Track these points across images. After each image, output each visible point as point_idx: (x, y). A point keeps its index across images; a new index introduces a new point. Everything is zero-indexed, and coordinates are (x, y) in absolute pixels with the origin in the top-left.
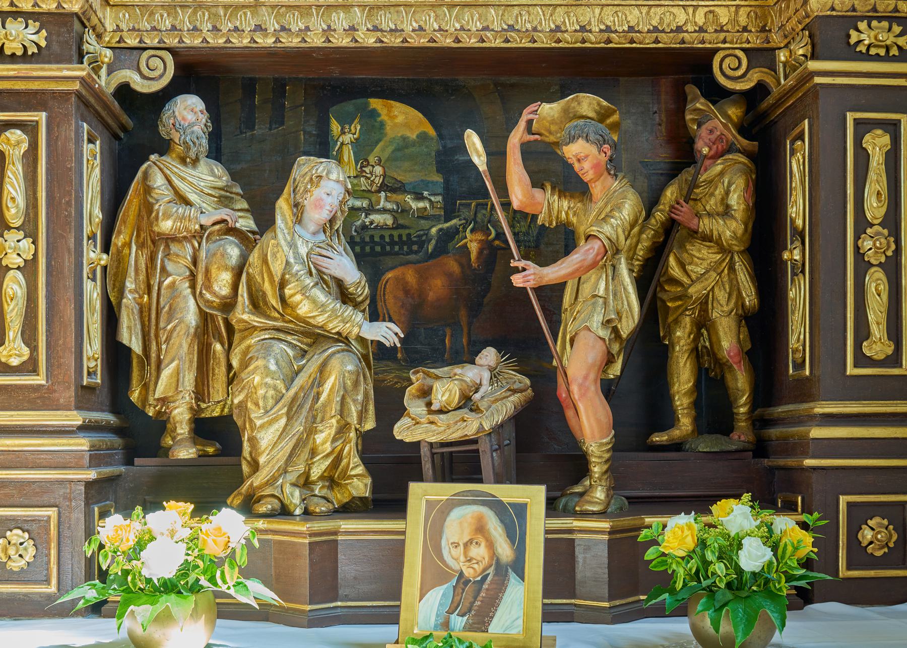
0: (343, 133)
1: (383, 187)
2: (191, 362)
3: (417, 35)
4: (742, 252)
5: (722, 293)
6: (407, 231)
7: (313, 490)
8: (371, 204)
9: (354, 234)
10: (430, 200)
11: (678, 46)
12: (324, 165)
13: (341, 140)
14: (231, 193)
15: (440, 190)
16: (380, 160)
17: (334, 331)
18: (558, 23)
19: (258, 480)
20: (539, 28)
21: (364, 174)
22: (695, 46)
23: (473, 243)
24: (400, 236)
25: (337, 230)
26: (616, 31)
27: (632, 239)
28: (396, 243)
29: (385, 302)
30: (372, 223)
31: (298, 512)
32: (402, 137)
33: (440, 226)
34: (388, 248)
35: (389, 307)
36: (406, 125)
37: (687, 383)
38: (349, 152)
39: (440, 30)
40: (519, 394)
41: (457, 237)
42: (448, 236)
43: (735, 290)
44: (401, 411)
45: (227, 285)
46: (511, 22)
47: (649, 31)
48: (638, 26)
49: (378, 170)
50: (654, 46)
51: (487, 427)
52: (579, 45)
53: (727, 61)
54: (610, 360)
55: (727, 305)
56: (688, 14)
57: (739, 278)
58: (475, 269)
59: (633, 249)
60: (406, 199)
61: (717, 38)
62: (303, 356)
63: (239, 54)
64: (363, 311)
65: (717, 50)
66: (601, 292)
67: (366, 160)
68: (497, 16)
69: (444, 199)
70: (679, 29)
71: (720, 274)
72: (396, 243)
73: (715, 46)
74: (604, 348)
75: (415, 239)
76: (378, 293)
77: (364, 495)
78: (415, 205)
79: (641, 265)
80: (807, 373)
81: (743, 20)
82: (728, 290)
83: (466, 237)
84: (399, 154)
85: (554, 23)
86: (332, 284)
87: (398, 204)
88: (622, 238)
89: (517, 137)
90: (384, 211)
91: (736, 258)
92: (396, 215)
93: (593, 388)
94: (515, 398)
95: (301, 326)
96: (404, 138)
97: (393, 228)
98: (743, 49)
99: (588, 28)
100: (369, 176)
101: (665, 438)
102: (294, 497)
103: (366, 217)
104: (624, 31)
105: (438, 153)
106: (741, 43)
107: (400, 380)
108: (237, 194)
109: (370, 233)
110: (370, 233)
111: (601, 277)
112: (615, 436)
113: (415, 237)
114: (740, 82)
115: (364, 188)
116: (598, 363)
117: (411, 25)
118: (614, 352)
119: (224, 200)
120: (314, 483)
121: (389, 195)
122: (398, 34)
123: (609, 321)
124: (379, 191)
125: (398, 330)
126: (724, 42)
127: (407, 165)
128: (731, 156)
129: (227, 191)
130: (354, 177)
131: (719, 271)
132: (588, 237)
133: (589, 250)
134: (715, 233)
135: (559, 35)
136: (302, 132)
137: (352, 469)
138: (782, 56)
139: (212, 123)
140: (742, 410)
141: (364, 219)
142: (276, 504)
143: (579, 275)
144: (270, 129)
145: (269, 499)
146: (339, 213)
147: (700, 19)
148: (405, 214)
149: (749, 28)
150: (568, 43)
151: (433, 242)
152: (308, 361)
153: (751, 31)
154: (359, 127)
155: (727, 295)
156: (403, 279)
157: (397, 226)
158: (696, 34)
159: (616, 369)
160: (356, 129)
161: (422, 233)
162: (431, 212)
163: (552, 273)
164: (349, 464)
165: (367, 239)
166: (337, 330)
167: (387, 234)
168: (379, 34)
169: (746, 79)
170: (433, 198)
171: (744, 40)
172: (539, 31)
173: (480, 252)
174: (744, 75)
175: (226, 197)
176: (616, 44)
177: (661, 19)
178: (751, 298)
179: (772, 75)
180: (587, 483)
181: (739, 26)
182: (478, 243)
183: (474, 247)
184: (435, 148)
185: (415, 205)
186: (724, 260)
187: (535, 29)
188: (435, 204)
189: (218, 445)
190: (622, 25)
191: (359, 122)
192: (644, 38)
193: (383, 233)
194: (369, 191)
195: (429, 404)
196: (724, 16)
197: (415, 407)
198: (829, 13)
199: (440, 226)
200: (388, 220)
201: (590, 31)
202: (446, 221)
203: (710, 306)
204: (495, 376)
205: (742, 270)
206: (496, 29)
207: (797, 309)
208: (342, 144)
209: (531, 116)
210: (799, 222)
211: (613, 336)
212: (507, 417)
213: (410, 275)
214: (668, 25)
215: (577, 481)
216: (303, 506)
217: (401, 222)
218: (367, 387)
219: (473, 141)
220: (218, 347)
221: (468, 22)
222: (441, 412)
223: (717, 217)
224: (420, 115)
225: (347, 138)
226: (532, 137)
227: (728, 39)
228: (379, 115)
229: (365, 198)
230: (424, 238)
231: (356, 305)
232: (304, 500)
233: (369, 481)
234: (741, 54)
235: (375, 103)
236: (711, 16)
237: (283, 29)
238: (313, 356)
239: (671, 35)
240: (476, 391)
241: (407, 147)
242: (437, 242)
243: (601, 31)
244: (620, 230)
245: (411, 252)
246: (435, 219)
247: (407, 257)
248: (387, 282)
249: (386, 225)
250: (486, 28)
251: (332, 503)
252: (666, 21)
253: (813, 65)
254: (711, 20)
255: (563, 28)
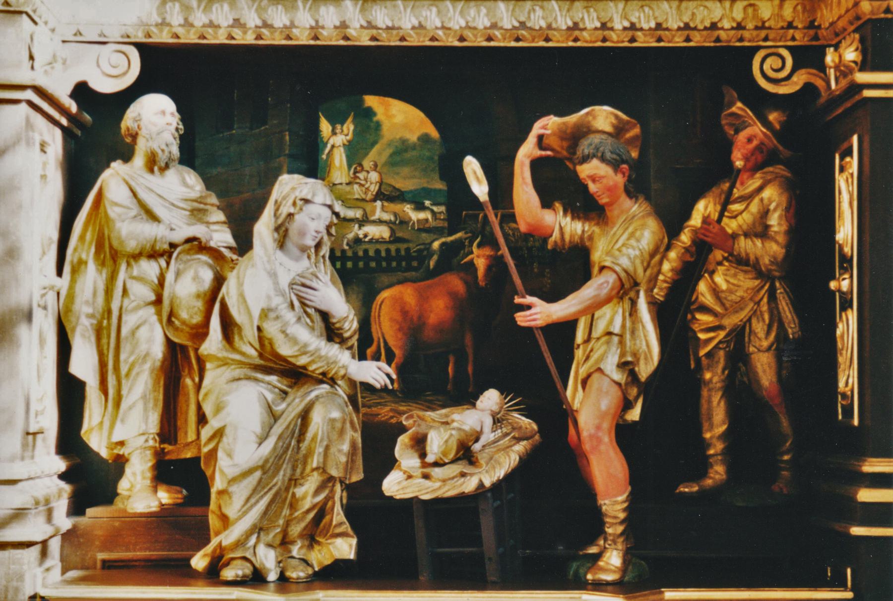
0: (334, 133)
1: (380, 196)
2: (156, 400)
3: (417, 34)
4: (780, 278)
5: (761, 324)
6: (405, 246)
7: (290, 551)
8: (365, 214)
9: (346, 247)
10: (432, 211)
11: (712, 44)
12: (309, 186)
13: (331, 142)
14: (206, 204)
15: (442, 200)
16: (376, 165)
17: (317, 372)
18: (577, 19)
19: (228, 538)
20: (554, 26)
21: (358, 181)
22: (732, 44)
23: (480, 259)
24: (398, 251)
25: (323, 257)
26: (641, 29)
27: (653, 268)
28: (393, 259)
29: (380, 325)
30: (366, 236)
31: (272, 577)
32: (401, 139)
33: (443, 240)
34: (384, 264)
35: (384, 331)
36: (405, 126)
37: (721, 425)
38: (341, 156)
39: (443, 28)
40: (524, 443)
41: (462, 252)
42: (451, 252)
43: (776, 317)
44: (390, 463)
45: (199, 314)
46: (522, 19)
47: (679, 29)
48: (667, 23)
49: (374, 176)
50: (685, 44)
51: (487, 483)
52: (599, 44)
53: (769, 61)
54: (627, 405)
55: (766, 338)
56: (725, 9)
57: (780, 307)
58: (483, 288)
59: (653, 281)
60: (405, 209)
61: (758, 36)
62: (284, 399)
63: (139, 560)
64: (350, 348)
65: (758, 48)
66: (616, 329)
67: (361, 165)
68: (507, 11)
69: (448, 210)
70: (714, 26)
71: (758, 303)
72: (393, 259)
73: (754, 44)
74: (620, 393)
75: (414, 254)
76: (372, 314)
77: (347, 557)
78: (415, 216)
79: (669, 288)
80: (856, 422)
81: (788, 12)
82: (767, 321)
83: (472, 253)
84: (398, 159)
85: (571, 19)
86: (317, 317)
87: (395, 215)
88: (640, 271)
89: (527, 151)
90: (380, 222)
91: (778, 284)
92: (394, 227)
93: (606, 439)
94: (521, 447)
95: (281, 365)
96: (404, 141)
97: (390, 242)
98: (788, 48)
99: (609, 25)
100: (363, 182)
101: (696, 489)
102: (267, 559)
103: (360, 228)
104: (650, 29)
105: (442, 158)
106: (786, 41)
107: (396, 415)
108: (212, 205)
109: (364, 247)
110: (364, 247)
111: (617, 312)
112: (631, 493)
113: (414, 252)
114: (782, 85)
115: (357, 196)
116: (612, 411)
117: (410, 21)
118: (631, 398)
119: (197, 213)
120: (293, 542)
121: (386, 204)
122: (395, 32)
123: (626, 364)
124: (374, 200)
125: (390, 370)
126: (766, 39)
127: (406, 170)
128: (771, 169)
129: (200, 203)
130: (347, 184)
131: (757, 299)
132: (602, 268)
133: (602, 284)
134: (752, 257)
135: (577, 33)
136: (287, 133)
137: (336, 526)
138: (830, 58)
139: (184, 125)
140: (786, 458)
141: (356, 231)
142: (248, 570)
143: (591, 309)
144: (251, 129)
145: (239, 562)
146: (326, 238)
147: (738, 13)
148: (405, 226)
149: (795, 24)
150: (586, 42)
151: (435, 257)
152: (289, 405)
153: (796, 28)
154: (352, 127)
155: (765, 327)
156: (401, 298)
157: (395, 239)
158: (733, 32)
159: (635, 414)
160: (349, 129)
161: (422, 247)
162: (432, 223)
163: (560, 310)
164: (331, 520)
165: (361, 254)
166: (321, 371)
167: (383, 248)
168: (374, 32)
169: (790, 82)
170: (435, 209)
171: (789, 37)
172: (555, 29)
173: (489, 269)
174: (789, 77)
175: (199, 210)
176: (642, 42)
177: (693, 14)
178: (794, 330)
179: (821, 78)
180: (602, 542)
181: (784, 20)
182: (486, 259)
183: (481, 264)
184: (438, 153)
185: (415, 216)
186: (762, 287)
187: (549, 27)
188: (438, 215)
189: (185, 492)
190: (648, 22)
191: (353, 122)
192: (674, 36)
193: (378, 246)
194: (363, 200)
195: (423, 455)
196: (766, 11)
197: (407, 459)
198: (882, 16)
199: (443, 240)
200: (382, 232)
201: (612, 29)
202: (450, 234)
203: (747, 339)
204: (497, 421)
205: (784, 298)
206: (506, 27)
207: (845, 348)
208: (333, 146)
209: (542, 131)
210: (847, 250)
211: (629, 379)
212: (510, 470)
213: (407, 293)
214: (702, 21)
215: (592, 542)
216: (279, 570)
217: (399, 234)
218: (354, 435)
219: (472, 166)
220: (188, 381)
221: (474, 19)
222: (436, 464)
223: (755, 239)
224: (421, 115)
225: (339, 140)
226: (543, 153)
227: (771, 37)
228: (375, 114)
229: (358, 207)
230: (425, 253)
231: (343, 341)
232: (280, 562)
233: (354, 541)
234: (785, 53)
235: (371, 101)
236: (750, 10)
237: (266, 25)
238: (294, 399)
239: (705, 33)
240: (477, 440)
241: (406, 150)
242: (440, 257)
243: (625, 29)
244: (638, 262)
245: (409, 268)
246: (438, 232)
247: (406, 274)
248: (382, 302)
249: (382, 238)
250: (494, 26)
251: (312, 566)
252: (699, 18)
253: (862, 77)
254: (750, 15)
255: (581, 26)
